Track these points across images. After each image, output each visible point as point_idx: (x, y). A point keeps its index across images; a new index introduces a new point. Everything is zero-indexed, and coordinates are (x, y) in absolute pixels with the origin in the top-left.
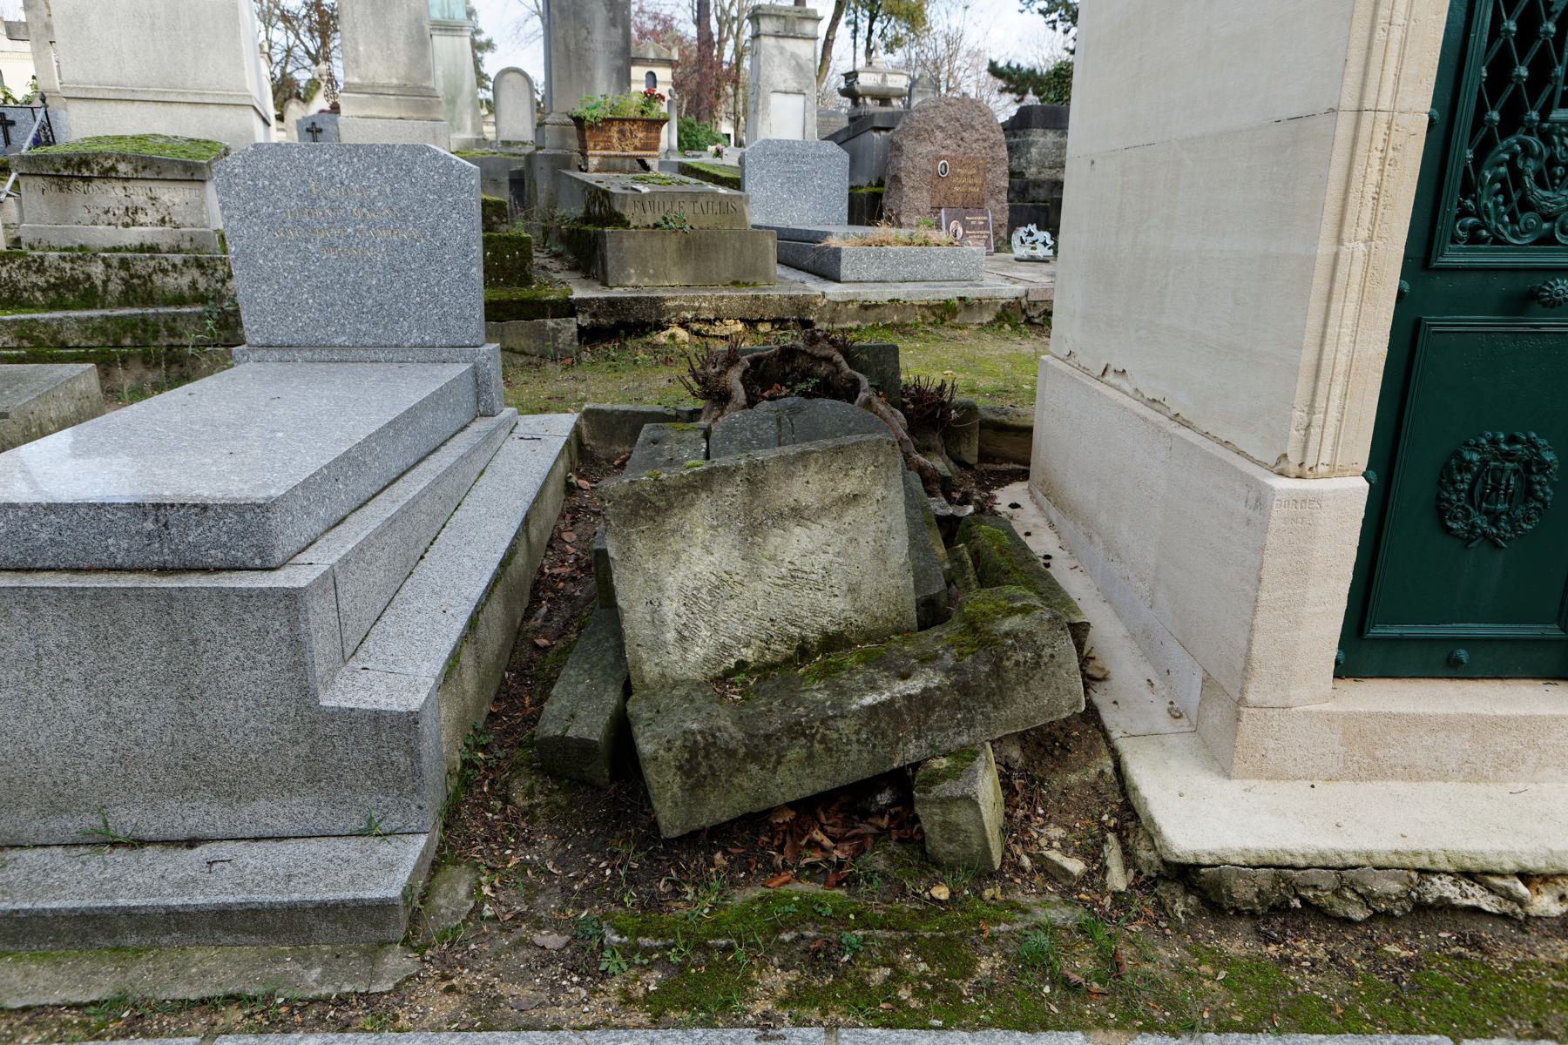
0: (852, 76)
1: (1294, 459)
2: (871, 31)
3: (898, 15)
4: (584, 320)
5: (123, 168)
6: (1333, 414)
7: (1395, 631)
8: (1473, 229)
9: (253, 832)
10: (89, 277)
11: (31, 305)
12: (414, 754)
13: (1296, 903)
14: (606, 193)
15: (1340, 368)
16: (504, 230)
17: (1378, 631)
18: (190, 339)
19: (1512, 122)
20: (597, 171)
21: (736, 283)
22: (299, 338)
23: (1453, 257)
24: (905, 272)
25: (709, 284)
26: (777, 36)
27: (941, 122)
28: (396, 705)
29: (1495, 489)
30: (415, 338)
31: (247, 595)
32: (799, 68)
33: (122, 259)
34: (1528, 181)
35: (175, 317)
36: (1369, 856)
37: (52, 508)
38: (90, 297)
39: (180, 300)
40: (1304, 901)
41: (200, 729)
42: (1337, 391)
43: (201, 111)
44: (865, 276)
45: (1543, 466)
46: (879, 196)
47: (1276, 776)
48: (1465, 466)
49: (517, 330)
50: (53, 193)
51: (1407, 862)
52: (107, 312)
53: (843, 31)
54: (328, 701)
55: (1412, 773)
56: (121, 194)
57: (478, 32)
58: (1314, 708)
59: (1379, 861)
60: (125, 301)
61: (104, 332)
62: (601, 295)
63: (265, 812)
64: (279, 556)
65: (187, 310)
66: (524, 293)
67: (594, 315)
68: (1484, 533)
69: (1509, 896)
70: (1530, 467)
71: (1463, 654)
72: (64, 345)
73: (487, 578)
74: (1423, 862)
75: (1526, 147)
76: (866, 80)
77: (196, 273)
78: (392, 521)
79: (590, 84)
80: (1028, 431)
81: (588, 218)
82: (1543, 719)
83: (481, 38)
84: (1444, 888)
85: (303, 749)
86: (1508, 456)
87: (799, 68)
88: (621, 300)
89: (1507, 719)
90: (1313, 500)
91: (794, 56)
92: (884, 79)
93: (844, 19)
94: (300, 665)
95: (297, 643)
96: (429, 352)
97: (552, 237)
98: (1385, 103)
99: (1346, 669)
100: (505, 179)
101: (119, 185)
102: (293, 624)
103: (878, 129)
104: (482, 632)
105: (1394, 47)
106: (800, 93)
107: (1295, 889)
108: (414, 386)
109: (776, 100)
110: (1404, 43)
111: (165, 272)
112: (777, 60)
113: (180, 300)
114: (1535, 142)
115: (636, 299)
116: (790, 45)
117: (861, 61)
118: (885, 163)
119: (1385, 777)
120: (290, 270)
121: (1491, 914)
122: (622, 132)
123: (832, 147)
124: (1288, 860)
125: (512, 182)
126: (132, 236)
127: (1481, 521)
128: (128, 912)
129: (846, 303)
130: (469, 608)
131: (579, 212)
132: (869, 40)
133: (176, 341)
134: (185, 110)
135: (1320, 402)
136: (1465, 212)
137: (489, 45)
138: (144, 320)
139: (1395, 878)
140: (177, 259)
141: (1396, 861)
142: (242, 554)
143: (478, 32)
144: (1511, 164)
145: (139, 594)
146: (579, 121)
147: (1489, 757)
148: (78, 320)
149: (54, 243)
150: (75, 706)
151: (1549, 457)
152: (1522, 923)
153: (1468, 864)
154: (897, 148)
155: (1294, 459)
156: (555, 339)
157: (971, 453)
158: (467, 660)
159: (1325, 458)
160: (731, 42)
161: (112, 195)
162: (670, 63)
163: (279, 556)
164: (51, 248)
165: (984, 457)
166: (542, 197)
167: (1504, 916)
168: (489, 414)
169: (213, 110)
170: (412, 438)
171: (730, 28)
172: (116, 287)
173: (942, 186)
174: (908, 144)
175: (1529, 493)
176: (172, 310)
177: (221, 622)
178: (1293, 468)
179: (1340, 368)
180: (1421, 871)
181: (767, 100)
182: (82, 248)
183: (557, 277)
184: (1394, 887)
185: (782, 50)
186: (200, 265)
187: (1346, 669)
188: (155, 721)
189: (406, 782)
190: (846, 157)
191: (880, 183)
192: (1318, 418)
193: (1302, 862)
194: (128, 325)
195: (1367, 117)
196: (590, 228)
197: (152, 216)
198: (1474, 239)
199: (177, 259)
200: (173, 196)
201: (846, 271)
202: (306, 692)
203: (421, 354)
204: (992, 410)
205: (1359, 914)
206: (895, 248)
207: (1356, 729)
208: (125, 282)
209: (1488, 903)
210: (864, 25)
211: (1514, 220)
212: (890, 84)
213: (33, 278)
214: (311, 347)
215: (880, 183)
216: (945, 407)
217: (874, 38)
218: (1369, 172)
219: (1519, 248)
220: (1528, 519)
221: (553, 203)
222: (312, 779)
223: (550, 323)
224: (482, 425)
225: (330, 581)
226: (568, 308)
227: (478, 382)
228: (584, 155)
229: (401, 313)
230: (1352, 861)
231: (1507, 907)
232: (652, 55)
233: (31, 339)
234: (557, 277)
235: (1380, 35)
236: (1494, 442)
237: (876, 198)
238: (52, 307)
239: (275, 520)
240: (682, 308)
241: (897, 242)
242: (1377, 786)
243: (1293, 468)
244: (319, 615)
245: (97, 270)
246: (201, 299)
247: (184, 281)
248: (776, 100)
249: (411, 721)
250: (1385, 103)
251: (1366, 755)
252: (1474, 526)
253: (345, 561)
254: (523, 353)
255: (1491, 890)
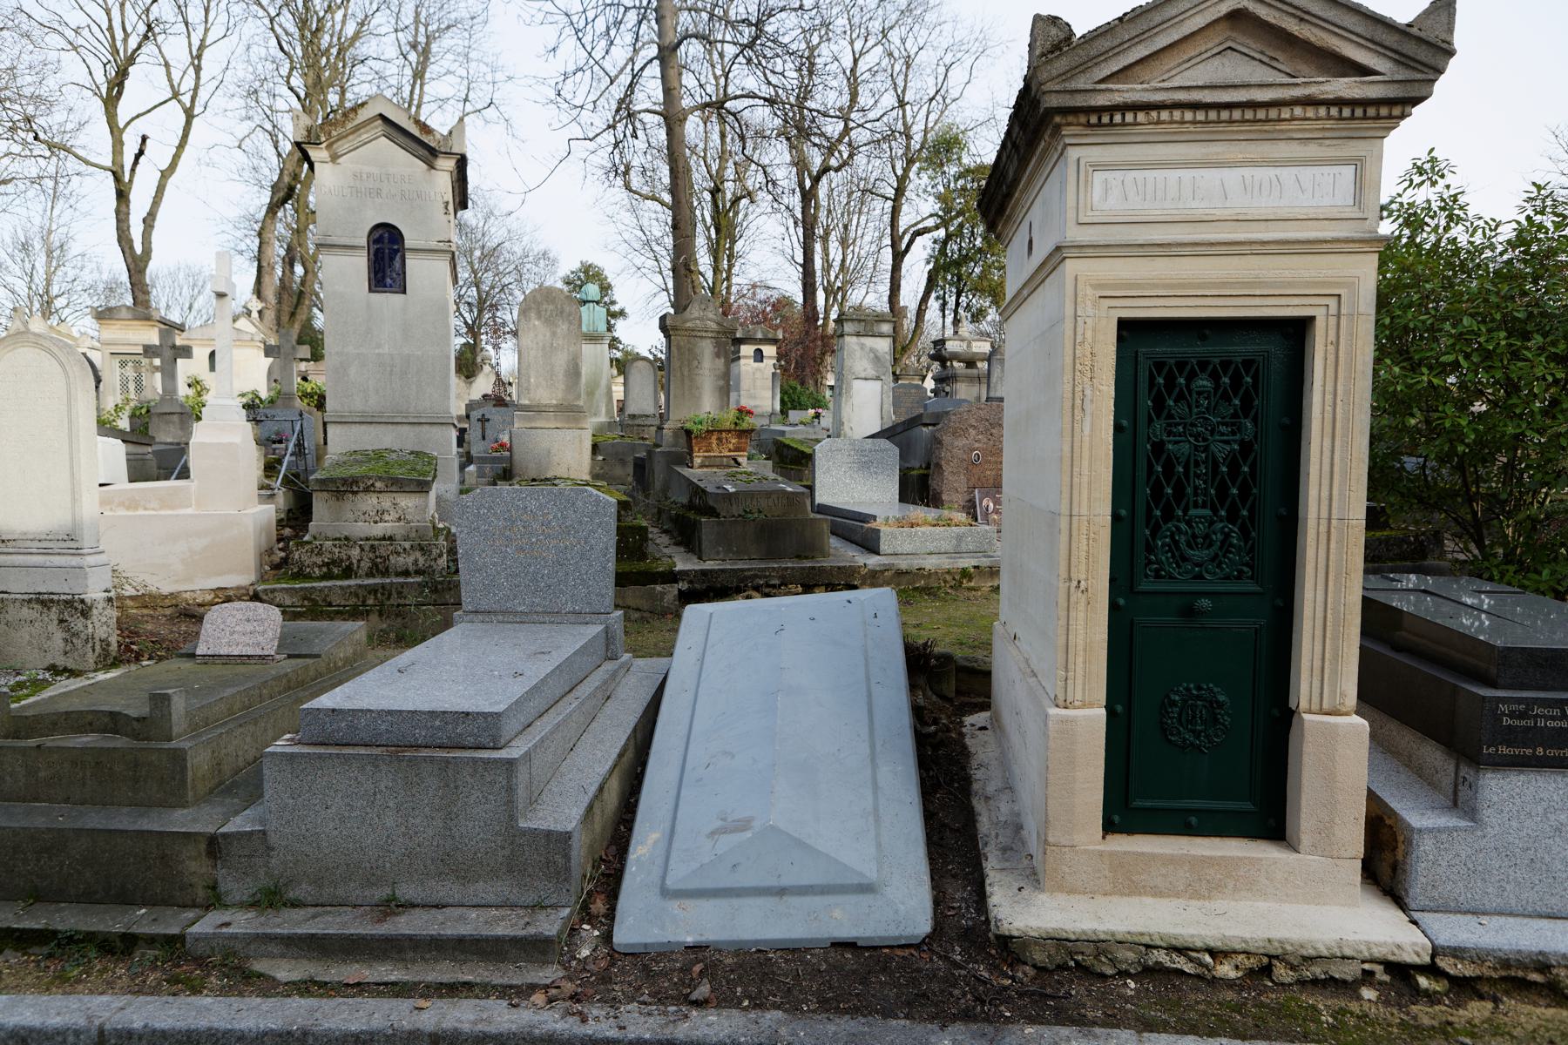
0: (940, 343)
1: (1061, 698)
2: (957, 304)
3: (982, 291)
4: (683, 586)
5: (378, 485)
6: (1080, 672)
7: (1148, 804)
8: (1157, 571)
9: (475, 901)
10: (349, 558)
11: (308, 577)
12: (567, 857)
13: (1072, 963)
14: (704, 491)
15: (1080, 647)
16: (629, 521)
17: (1138, 803)
18: (411, 600)
19: (1168, 515)
20: (701, 466)
21: (798, 557)
22: (496, 607)
23: (1145, 586)
24: (931, 547)
25: (778, 556)
26: (858, 335)
27: (973, 422)
28: (560, 828)
29: (1194, 717)
30: (569, 607)
31: (487, 762)
32: (877, 359)
33: (373, 545)
34: (1183, 546)
35: (402, 585)
36: (1113, 935)
37: (390, 712)
38: (348, 572)
39: (406, 573)
40: (1077, 962)
41: (453, 838)
42: (1080, 660)
43: (417, 429)
44: (900, 550)
45: (1221, 705)
46: (927, 476)
47: (1072, 891)
48: (1173, 704)
49: (634, 594)
50: (332, 502)
51: (1136, 939)
52: (359, 582)
53: (934, 305)
54: (523, 824)
55: (1157, 893)
56: (375, 501)
57: (613, 303)
58: (1091, 847)
59: (1119, 938)
60: (370, 575)
61: (357, 596)
62: (697, 568)
63: (484, 890)
64: (503, 741)
65: (410, 580)
66: (642, 566)
67: (691, 582)
68: (1192, 744)
69: (1201, 964)
70: (1213, 704)
71: (1194, 820)
72: (330, 605)
73: (610, 763)
74: (1146, 940)
75: (1178, 529)
76: (952, 346)
77: (418, 554)
78: (558, 725)
79: (697, 400)
80: (988, 674)
81: (690, 506)
82: (1233, 858)
83: (616, 308)
84: (1161, 957)
85: (507, 852)
86: (1198, 697)
87: (877, 359)
88: (711, 571)
89: (1211, 858)
90: (1073, 720)
91: (872, 350)
92: (969, 345)
93: (933, 295)
94: (510, 802)
95: (510, 789)
96: (579, 617)
97: (664, 516)
98: (1084, 511)
99: (1109, 827)
100: (630, 459)
101: (374, 496)
102: (509, 779)
103: (926, 425)
104: (605, 795)
105: (1085, 485)
106: (878, 378)
107: (1071, 954)
108: (572, 640)
109: (857, 384)
110: (1090, 483)
111: (398, 554)
112: (858, 354)
113: (406, 573)
114: (1183, 526)
115: (723, 571)
116: (869, 342)
117: (949, 332)
118: (930, 452)
119: (1140, 894)
120: (495, 564)
121: (1190, 975)
122: (719, 439)
123: (884, 443)
124: (1065, 935)
125: (636, 465)
126: (379, 530)
127: (1189, 737)
128: (410, 938)
129: (882, 572)
130: (600, 779)
131: (684, 500)
132: (956, 312)
133: (402, 602)
134: (406, 428)
135: (1071, 666)
136: (1150, 562)
137: (622, 313)
138: (383, 586)
139: (1130, 949)
140: (407, 545)
141: (1129, 938)
142: (483, 740)
143: (613, 303)
144: (1172, 536)
145: (432, 759)
146: (688, 433)
147: (1201, 885)
148: (341, 587)
149: (329, 535)
150: (389, 822)
151: (1221, 698)
152: (1215, 982)
153: (1174, 942)
154: (937, 442)
155: (1061, 698)
156: (662, 599)
157: (950, 688)
158: (597, 811)
159: (1079, 696)
160: (836, 308)
161: (370, 502)
162: (774, 341)
163: (503, 741)
164: (327, 539)
165: (959, 692)
166: (658, 485)
167: (1198, 977)
168: (614, 658)
169: (427, 427)
170: (569, 679)
171: (835, 299)
172: (366, 565)
173: (976, 471)
174: (947, 439)
175: (1216, 721)
176: (401, 580)
177: (472, 776)
178: (1061, 703)
179: (1080, 647)
180: (1148, 946)
181: (850, 387)
182: (347, 538)
183: (666, 551)
184: (1131, 955)
185: (862, 346)
186: (422, 549)
187: (1109, 827)
188: (430, 832)
189: (560, 874)
190: (897, 450)
191: (928, 467)
192: (1071, 674)
193: (1073, 937)
194: (373, 590)
195: (1075, 519)
196: (692, 515)
197: (393, 516)
198: (1158, 576)
199: (407, 545)
200: (407, 502)
201: (884, 547)
202: (512, 818)
203: (572, 618)
204: (966, 659)
205: (1110, 971)
206: (923, 529)
207: (1119, 863)
208: (372, 561)
209: (1188, 968)
210: (952, 301)
211: (1179, 566)
212: (975, 350)
213: (315, 559)
214: (503, 613)
215: (928, 467)
216: (927, 657)
217: (961, 311)
218: (1081, 546)
219: (1211, 582)
220: (1217, 736)
221: (666, 489)
222: (510, 871)
223: (659, 588)
224: (609, 666)
225: (528, 756)
226: (671, 577)
227: (608, 635)
228: (691, 452)
229: (562, 592)
230: (1103, 937)
231: (1199, 970)
232: (759, 336)
233: (309, 599)
234: (666, 551)
235: (1076, 480)
236: (1188, 689)
237: (924, 480)
238: (323, 578)
239: (504, 720)
240: (756, 576)
241: (926, 523)
242: (1135, 900)
243: (1061, 703)
244: (522, 776)
245: (355, 552)
246: (418, 572)
247: (410, 560)
248: (857, 384)
249: (566, 837)
250: (1084, 511)
251: (1127, 882)
252: (1185, 740)
253: (535, 746)
254: (638, 610)
255: (1191, 960)
